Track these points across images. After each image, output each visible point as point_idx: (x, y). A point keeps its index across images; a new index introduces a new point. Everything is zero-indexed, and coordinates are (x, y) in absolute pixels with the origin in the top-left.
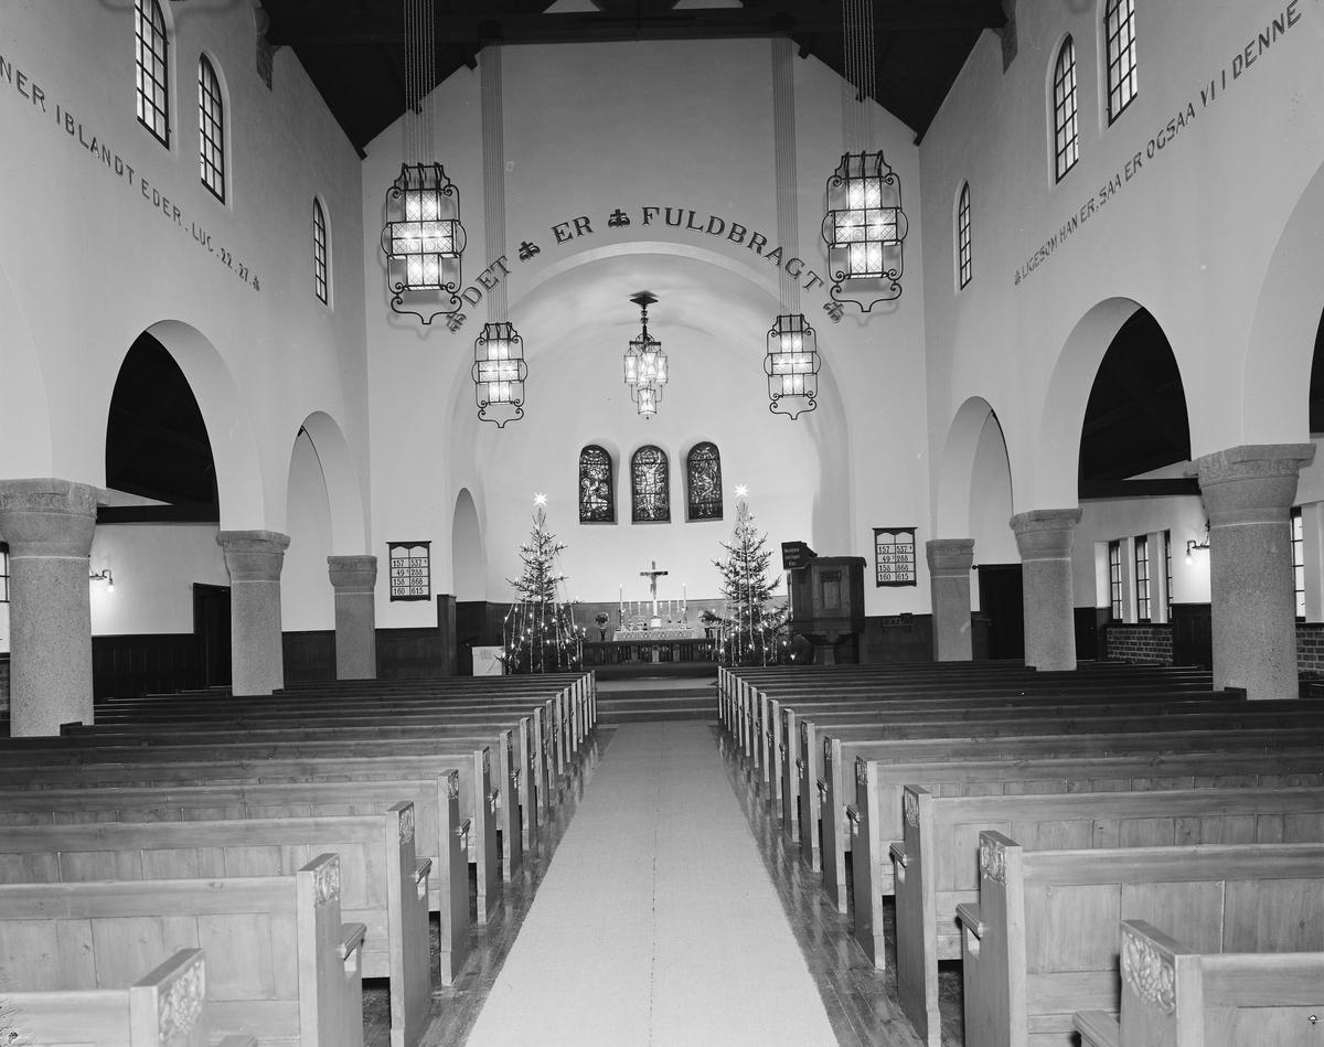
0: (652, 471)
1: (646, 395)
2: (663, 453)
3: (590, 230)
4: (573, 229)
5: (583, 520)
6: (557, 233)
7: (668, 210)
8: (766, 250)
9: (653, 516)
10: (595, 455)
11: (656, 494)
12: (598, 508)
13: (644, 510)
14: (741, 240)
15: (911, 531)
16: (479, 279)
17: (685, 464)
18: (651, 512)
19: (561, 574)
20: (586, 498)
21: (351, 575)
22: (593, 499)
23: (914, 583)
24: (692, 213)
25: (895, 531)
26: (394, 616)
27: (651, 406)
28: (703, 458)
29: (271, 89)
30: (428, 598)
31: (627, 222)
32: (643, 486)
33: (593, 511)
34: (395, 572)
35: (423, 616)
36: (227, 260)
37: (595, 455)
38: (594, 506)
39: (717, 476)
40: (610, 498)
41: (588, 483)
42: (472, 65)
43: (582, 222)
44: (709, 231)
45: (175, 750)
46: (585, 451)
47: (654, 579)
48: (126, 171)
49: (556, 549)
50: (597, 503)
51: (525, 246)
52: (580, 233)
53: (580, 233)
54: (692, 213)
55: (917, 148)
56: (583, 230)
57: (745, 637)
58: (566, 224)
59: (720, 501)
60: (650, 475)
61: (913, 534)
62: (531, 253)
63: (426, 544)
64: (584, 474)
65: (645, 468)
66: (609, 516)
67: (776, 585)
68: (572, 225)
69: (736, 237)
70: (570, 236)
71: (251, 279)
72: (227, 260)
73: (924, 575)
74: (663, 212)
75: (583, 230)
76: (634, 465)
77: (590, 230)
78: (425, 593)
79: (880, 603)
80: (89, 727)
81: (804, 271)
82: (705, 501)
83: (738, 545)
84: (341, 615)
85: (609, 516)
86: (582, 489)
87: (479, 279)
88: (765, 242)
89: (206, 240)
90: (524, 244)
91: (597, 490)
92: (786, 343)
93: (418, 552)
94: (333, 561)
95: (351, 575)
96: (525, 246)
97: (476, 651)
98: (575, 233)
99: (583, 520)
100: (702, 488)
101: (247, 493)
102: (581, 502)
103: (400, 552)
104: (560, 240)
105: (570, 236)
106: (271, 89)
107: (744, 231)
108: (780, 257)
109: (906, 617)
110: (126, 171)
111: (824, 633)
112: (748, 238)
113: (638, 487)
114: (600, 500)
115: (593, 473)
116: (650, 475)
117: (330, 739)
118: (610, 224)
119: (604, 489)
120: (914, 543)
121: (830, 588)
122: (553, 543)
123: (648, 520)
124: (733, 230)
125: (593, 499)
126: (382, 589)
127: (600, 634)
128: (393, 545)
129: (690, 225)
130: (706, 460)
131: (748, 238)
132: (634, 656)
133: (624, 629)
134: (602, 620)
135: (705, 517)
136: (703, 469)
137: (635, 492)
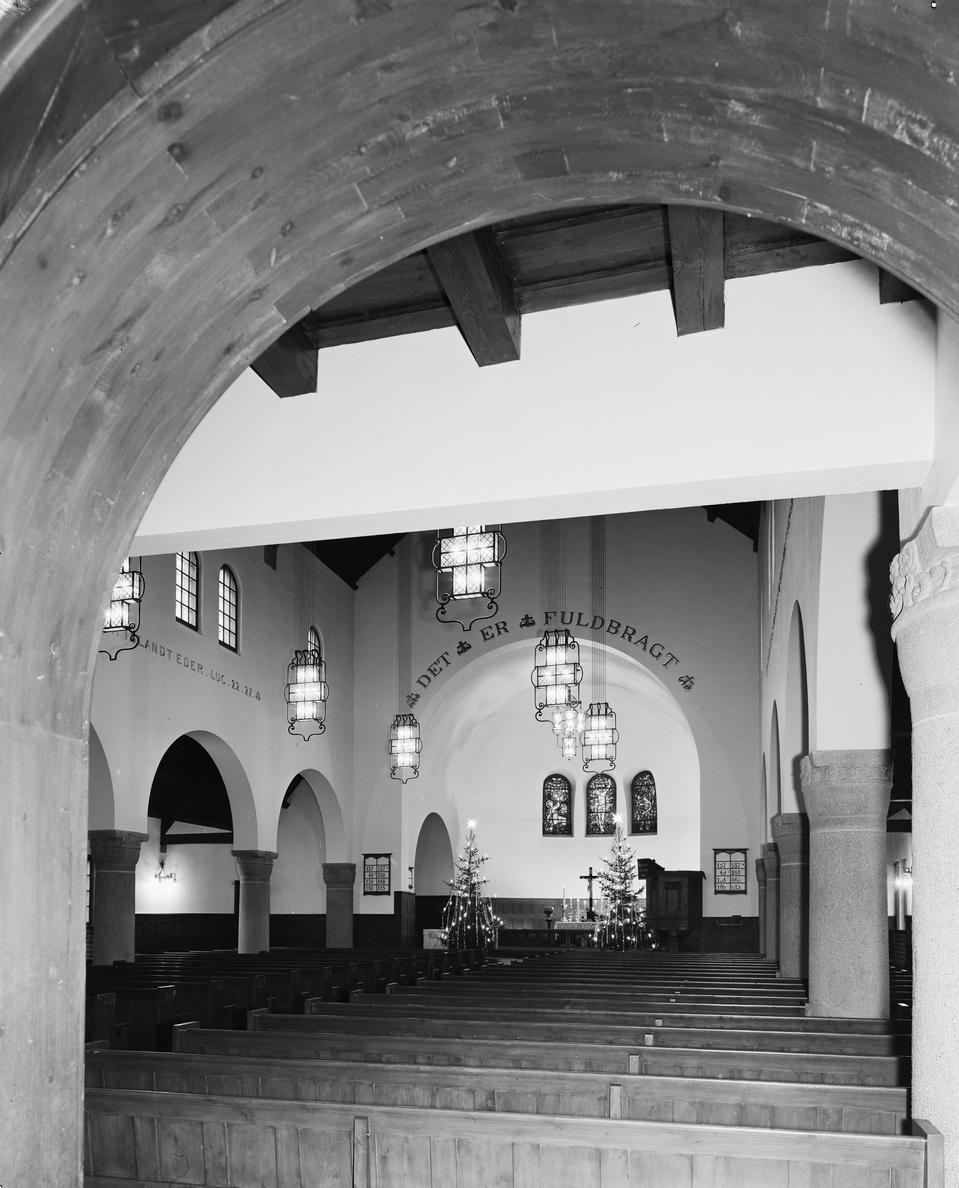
0: (604, 794)
1: (569, 742)
2: (612, 780)
3: (506, 630)
4: (494, 630)
5: (545, 833)
6: (483, 634)
7: (563, 613)
8: (635, 638)
9: (603, 830)
10: (557, 782)
11: (606, 812)
12: (559, 824)
13: (596, 825)
14: (617, 631)
15: (744, 851)
16: (429, 669)
17: (629, 788)
18: (601, 827)
19: (484, 879)
20: (549, 816)
21: (339, 877)
22: (555, 816)
23: (745, 892)
24: (580, 614)
25: (730, 851)
26: (368, 906)
27: (584, 744)
28: (643, 784)
29: (274, 568)
30: (388, 893)
31: (470, 647)
32: (596, 806)
33: (555, 826)
34: (367, 874)
35: (385, 906)
36: (236, 686)
37: (557, 782)
38: (556, 822)
39: (654, 799)
40: (569, 816)
41: (551, 804)
42: (392, 554)
43: (501, 625)
44: (593, 627)
45: (486, 1045)
46: (549, 779)
47: (590, 882)
48: (167, 653)
49: (483, 860)
50: (558, 820)
51: (461, 644)
52: (499, 633)
53: (499, 633)
54: (580, 614)
55: (755, 554)
56: (502, 631)
57: (611, 928)
58: (490, 627)
59: (655, 819)
60: (602, 797)
61: (745, 854)
62: (465, 650)
63: (388, 856)
64: (547, 797)
65: (597, 792)
66: (568, 830)
67: (641, 891)
68: (494, 627)
69: (613, 630)
70: (493, 636)
71: (254, 694)
72: (236, 686)
73: (753, 886)
74: (559, 615)
75: (502, 631)
76: (589, 790)
77: (506, 630)
78: (387, 890)
79: (715, 907)
80: (131, 964)
81: (664, 653)
82: (645, 819)
83: (613, 860)
84: (330, 903)
85: (568, 830)
86: (546, 809)
87: (429, 669)
88: (634, 632)
89: (220, 678)
90: (460, 643)
91: (559, 809)
92: (595, 722)
93: (383, 861)
94: (326, 867)
95: (339, 877)
96: (461, 644)
97: (426, 932)
98: (496, 634)
99: (545, 833)
100: (643, 808)
101: (261, 820)
102: (544, 818)
103: (371, 861)
104: (485, 639)
105: (493, 636)
106: (274, 568)
107: (619, 625)
108: (645, 644)
109: (737, 919)
110: (167, 653)
111: (666, 928)
112: (622, 630)
113: (592, 807)
114: (560, 818)
115: (556, 796)
116: (602, 797)
117: (524, 1020)
118: (521, 626)
119: (564, 809)
120: (746, 861)
121: (673, 893)
122: (479, 855)
123: (599, 833)
124: (611, 626)
125: (555, 816)
126: (358, 887)
127: (546, 923)
128: (367, 856)
129: (578, 624)
130: (647, 785)
131: (622, 630)
132: (568, 941)
133: (565, 920)
134: (548, 912)
135: (645, 832)
136: (644, 793)
137: (589, 811)
